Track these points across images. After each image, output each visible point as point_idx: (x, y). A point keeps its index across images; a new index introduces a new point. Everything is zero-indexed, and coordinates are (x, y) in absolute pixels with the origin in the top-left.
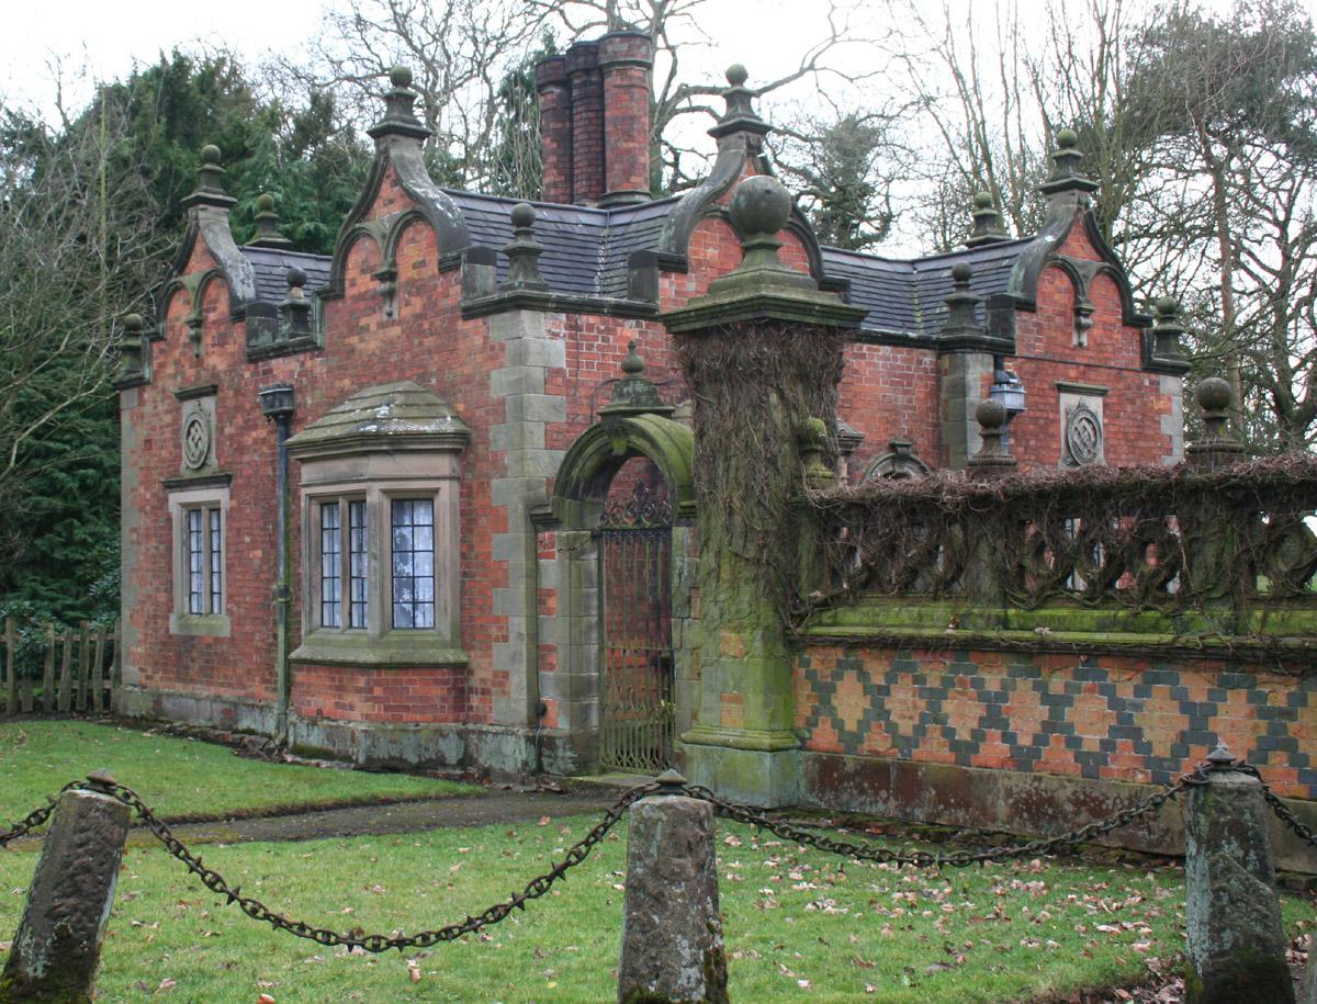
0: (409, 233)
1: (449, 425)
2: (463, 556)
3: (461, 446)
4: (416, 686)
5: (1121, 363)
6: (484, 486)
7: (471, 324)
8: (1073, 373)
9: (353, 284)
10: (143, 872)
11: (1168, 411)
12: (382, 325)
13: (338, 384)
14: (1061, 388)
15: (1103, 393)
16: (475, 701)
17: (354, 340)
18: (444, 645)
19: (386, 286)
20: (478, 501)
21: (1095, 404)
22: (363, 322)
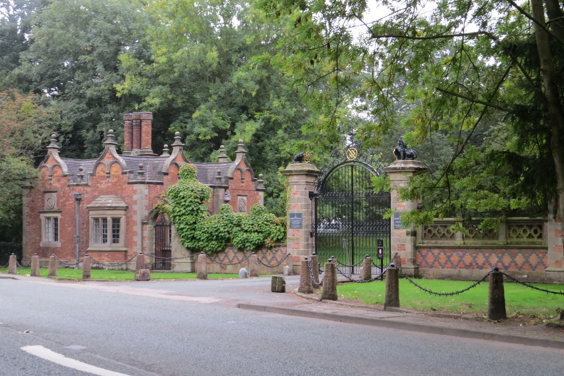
0: (114, 165)
1: (123, 205)
3: (126, 209)
4: (118, 255)
6: (131, 217)
8: (241, 192)
9: (98, 173)
10: (189, 269)
11: (260, 199)
12: (106, 183)
13: (94, 194)
14: (238, 195)
15: (246, 196)
17: (99, 185)
18: (122, 247)
19: (108, 175)
20: (130, 219)
21: (245, 198)
22: (101, 181)
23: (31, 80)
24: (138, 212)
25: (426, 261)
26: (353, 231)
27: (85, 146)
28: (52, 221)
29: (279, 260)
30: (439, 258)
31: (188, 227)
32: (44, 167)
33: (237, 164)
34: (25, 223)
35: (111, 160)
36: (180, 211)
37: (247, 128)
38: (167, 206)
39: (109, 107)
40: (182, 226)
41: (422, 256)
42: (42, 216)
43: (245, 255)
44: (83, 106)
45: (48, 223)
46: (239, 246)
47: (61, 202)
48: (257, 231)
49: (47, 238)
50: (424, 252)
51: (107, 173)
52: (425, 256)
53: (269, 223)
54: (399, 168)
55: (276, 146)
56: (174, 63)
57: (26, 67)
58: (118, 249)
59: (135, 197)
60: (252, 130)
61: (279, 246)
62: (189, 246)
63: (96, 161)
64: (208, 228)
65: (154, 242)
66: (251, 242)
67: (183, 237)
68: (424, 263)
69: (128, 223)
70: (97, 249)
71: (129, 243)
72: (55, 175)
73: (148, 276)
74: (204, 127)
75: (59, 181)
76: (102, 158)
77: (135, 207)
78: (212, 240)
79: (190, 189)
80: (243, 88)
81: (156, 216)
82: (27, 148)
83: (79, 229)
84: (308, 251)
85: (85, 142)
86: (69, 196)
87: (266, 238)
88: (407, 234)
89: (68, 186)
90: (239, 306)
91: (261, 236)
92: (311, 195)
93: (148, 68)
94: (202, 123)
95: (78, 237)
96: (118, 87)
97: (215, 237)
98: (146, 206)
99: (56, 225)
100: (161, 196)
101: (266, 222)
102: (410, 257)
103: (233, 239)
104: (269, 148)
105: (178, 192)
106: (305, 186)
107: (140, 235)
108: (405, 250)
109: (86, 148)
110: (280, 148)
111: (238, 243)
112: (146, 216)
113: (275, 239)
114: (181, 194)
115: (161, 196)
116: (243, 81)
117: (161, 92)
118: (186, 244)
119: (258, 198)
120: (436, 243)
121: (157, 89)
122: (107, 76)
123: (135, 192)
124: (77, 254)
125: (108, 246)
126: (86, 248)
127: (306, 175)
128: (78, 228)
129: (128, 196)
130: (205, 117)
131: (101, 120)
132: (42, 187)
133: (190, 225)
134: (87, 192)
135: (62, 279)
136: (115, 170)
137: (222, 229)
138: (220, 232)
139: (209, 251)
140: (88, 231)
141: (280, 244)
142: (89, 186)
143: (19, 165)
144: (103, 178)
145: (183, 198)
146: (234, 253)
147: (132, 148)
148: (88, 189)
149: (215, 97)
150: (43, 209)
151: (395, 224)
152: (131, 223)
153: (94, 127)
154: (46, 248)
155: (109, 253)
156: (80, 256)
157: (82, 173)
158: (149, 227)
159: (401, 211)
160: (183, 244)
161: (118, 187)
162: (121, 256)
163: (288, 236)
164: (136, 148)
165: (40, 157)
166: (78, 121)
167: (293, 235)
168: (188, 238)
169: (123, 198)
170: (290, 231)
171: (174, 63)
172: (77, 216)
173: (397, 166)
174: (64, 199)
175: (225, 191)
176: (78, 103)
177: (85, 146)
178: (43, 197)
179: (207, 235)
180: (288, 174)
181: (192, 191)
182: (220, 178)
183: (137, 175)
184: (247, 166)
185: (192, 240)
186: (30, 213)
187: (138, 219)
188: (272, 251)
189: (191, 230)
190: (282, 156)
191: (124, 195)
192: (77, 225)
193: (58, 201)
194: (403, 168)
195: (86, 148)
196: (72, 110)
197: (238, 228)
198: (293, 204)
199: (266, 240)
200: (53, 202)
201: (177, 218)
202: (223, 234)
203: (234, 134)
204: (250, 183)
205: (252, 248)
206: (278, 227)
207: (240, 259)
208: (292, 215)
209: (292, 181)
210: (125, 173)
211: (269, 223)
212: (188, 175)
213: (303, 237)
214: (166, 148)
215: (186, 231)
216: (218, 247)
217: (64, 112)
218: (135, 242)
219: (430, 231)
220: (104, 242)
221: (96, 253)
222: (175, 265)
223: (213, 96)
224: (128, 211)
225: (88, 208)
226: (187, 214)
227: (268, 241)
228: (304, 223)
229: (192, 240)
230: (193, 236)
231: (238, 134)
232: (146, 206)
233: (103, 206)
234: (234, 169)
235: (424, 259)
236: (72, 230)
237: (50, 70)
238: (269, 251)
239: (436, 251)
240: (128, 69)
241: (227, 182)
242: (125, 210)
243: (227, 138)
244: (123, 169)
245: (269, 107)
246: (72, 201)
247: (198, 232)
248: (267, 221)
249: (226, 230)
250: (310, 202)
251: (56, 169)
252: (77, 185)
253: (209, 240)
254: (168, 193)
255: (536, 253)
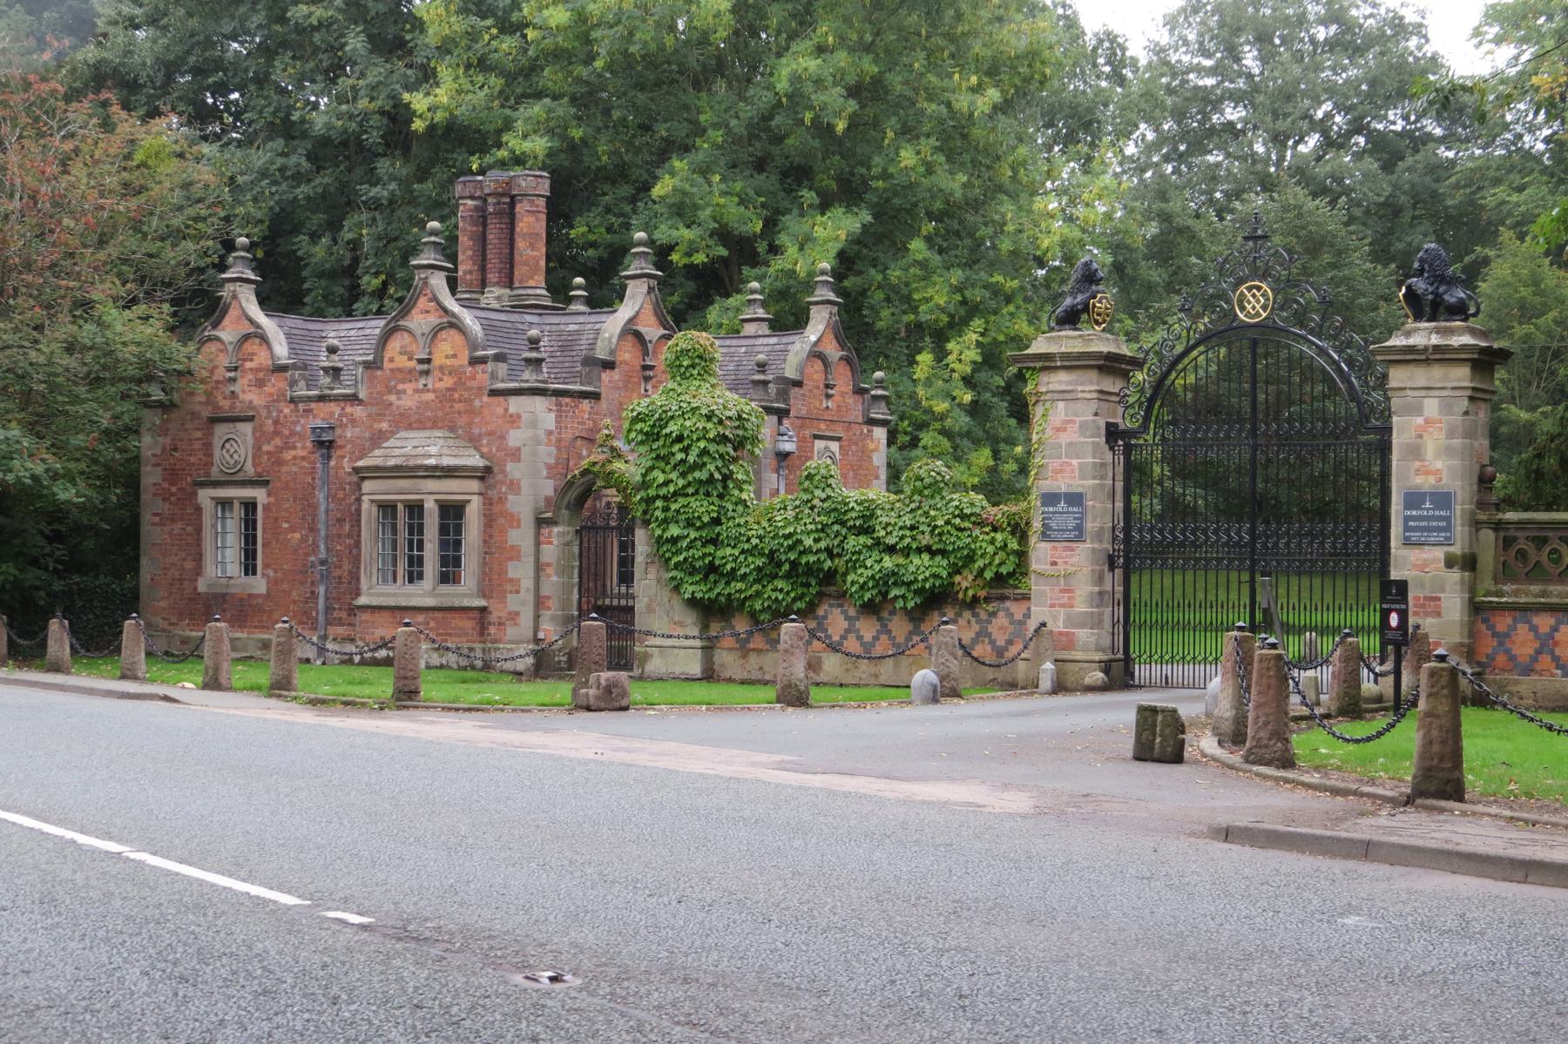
0: (444, 334)
1: (476, 461)
2: (485, 541)
3: (484, 474)
5: (851, 419)
6: (502, 500)
7: (492, 399)
8: (823, 426)
9: (391, 360)
10: (696, 669)
11: (876, 450)
12: (417, 391)
14: (816, 437)
15: (839, 439)
16: (492, 630)
17: (393, 398)
18: (471, 596)
19: (425, 367)
20: (496, 509)
21: (834, 446)
22: (400, 387)
23: (135, 80)
24: (523, 484)
25: (1508, 652)
26: (1253, 552)
27: (306, 286)
28: (238, 511)
29: (1001, 643)
30: (1556, 644)
31: (693, 535)
32: (210, 339)
33: (813, 338)
34: (147, 518)
35: (434, 319)
36: (667, 483)
37: (819, 232)
38: (618, 465)
39: (383, 166)
40: (674, 531)
41: (1495, 635)
42: (205, 496)
43: (884, 626)
44: (298, 161)
45: (224, 518)
46: (868, 596)
47: (269, 453)
48: (928, 549)
49: (222, 562)
50: (1503, 622)
51: (421, 361)
52: (1507, 635)
53: (967, 524)
54: (1426, 349)
55: (905, 291)
56: (594, 26)
57: (120, 40)
58: (457, 603)
59: (515, 438)
60: (837, 238)
61: (1003, 598)
62: (699, 595)
63: (382, 323)
64: (760, 538)
65: (576, 580)
66: (909, 584)
67: (677, 566)
68: (1501, 659)
69: (489, 520)
70: (391, 602)
71: (492, 583)
72: (248, 365)
73: (624, 694)
74: (688, 227)
75: (260, 384)
76: (404, 313)
77: (513, 470)
78: (776, 576)
79: (704, 411)
80: (812, 108)
81: (579, 495)
82: (145, 284)
83: (327, 536)
84: (1101, 614)
85: (304, 273)
86: (293, 434)
87: (958, 572)
88: (1450, 563)
89: (292, 400)
90: (1228, 834)
91: (941, 566)
92: (1113, 433)
93: (508, 44)
94: (680, 215)
95: (323, 563)
96: (418, 101)
97: (787, 567)
98: (549, 467)
99: (250, 524)
100: (599, 437)
101: (958, 521)
102: (1458, 639)
103: (845, 574)
104: (880, 295)
105: (663, 422)
106: (1094, 405)
107: (532, 559)
108: (1439, 614)
109: (309, 290)
110: (916, 296)
111: (862, 587)
112: (548, 499)
113: (988, 575)
114: (673, 428)
115: (599, 437)
116: (809, 87)
117: (548, 120)
118: (688, 590)
119: (872, 446)
120: (1543, 594)
121: (537, 109)
122: (376, 72)
123: (514, 420)
124: (321, 618)
125: (425, 593)
126: (357, 598)
127: (1100, 368)
128: (323, 533)
129: (490, 434)
130: (692, 194)
131: (351, 205)
132: (208, 403)
133: (699, 529)
134: (353, 421)
135: (323, 702)
136: (448, 349)
137: (808, 542)
138: (801, 553)
139: (763, 610)
140: (358, 544)
141: (1006, 592)
142: (361, 402)
143: (137, 331)
144: (409, 375)
145: (680, 439)
146: (847, 618)
147: (484, 283)
148: (358, 411)
149: (717, 136)
150: (208, 474)
151: (1407, 529)
152: (502, 521)
153: (334, 226)
154: (215, 596)
155: (431, 614)
156: (328, 623)
157: (336, 361)
158: (558, 534)
159: (1426, 489)
160: (676, 589)
161: (457, 406)
162: (468, 624)
163: (1035, 565)
164: (497, 284)
165: (197, 306)
166: (282, 210)
167: (1054, 563)
168: (693, 571)
169: (474, 442)
170: (1041, 554)
171: (594, 26)
172: (321, 496)
173: (1418, 340)
174: (278, 441)
175: (780, 423)
176: (283, 154)
177: (306, 286)
178: (209, 434)
179: (760, 562)
180: (1039, 365)
181: (709, 418)
182: (765, 383)
183: (520, 370)
184: (842, 347)
185: (706, 577)
186: (166, 485)
187: (523, 505)
188: (975, 615)
189: (704, 545)
190: (923, 318)
191: (476, 431)
192: (321, 526)
193: (257, 448)
194: (1436, 348)
195: (309, 290)
196: (264, 174)
197: (862, 539)
198: (1054, 464)
199: (957, 579)
200: (242, 452)
201: (659, 503)
202: (812, 559)
203: (775, 250)
204: (851, 400)
205: (910, 605)
206: (999, 536)
207: (868, 637)
208: (1050, 499)
209: (1051, 387)
210: (483, 360)
211: (967, 524)
212: (693, 366)
213: (1087, 570)
214: (579, 288)
215: (689, 548)
216: (794, 600)
217: (240, 179)
218: (515, 582)
219: (1522, 554)
220: (411, 581)
221: (386, 614)
222: (646, 657)
223: (710, 132)
224: (491, 481)
225: (356, 470)
226: (690, 490)
227: (964, 581)
228: (1090, 525)
229: (706, 577)
230: (711, 563)
231: (792, 251)
232: (549, 467)
233: (411, 463)
234: (804, 355)
235: (1501, 644)
236: (303, 540)
237: (197, 51)
238: (967, 614)
239: (1544, 622)
240: (444, 49)
241: (783, 395)
242: (482, 478)
243: (754, 260)
244: (473, 345)
245: (885, 170)
246: (303, 448)
247: (729, 551)
248: (963, 517)
249: (822, 545)
250: (1109, 456)
251: (252, 346)
252: (322, 398)
253: (762, 576)
254: (626, 425)
255: (1528, 622)
